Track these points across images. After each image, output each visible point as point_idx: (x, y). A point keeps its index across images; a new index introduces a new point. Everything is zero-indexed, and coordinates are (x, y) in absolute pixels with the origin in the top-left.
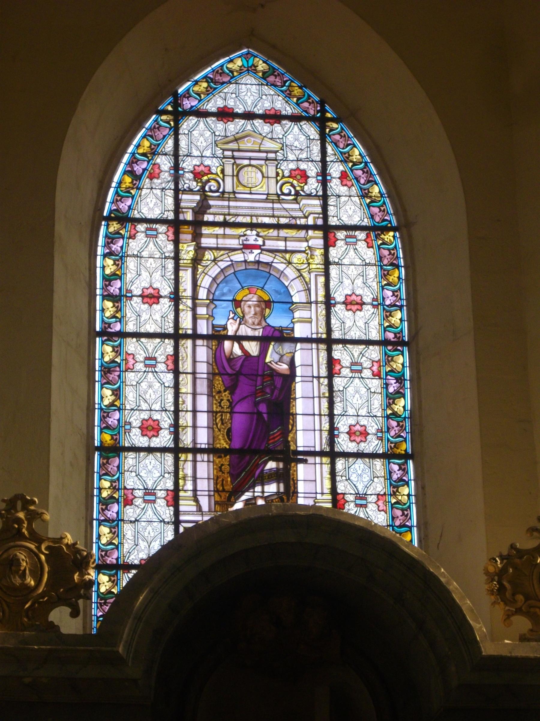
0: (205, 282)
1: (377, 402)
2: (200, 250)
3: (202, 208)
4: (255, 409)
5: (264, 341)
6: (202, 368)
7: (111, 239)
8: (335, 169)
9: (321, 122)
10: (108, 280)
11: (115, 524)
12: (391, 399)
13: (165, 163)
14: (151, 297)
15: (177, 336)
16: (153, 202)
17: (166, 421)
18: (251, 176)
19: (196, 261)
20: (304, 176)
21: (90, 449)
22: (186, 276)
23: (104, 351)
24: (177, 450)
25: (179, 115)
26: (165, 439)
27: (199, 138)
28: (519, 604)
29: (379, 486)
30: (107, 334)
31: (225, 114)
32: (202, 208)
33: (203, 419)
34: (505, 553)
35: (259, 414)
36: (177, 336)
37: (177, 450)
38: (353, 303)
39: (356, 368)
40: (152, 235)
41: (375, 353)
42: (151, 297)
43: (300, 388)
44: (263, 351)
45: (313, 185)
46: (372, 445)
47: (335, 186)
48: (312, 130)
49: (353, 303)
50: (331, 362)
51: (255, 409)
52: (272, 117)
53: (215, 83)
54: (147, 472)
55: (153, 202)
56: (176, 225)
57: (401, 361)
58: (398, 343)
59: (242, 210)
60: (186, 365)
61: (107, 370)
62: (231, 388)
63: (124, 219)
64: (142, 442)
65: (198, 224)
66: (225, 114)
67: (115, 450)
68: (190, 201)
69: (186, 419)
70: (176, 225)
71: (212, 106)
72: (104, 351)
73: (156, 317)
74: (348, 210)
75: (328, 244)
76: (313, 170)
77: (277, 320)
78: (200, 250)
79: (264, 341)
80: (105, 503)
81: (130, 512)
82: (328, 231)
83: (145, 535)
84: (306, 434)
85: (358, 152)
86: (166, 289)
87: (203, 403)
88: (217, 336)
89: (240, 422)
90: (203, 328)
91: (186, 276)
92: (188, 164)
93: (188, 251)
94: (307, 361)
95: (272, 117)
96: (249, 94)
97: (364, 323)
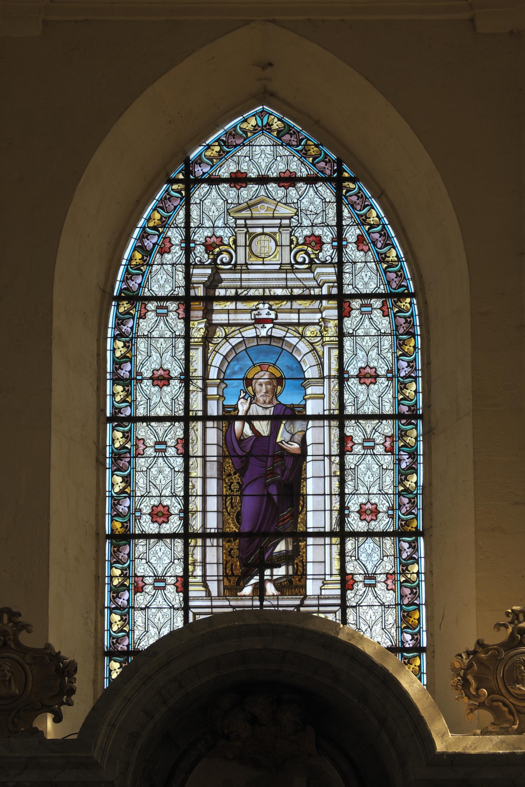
0: (217, 360)
1: (389, 478)
2: (211, 327)
3: (214, 282)
5: (275, 420)
6: (212, 451)
7: (120, 321)
8: (352, 234)
9: (337, 182)
10: (118, 363)
11: (126, 612)
12: (402, 475)
13: (176, 236)
14: (161, 379)
15: (187, 419)
16: (163, 280)
17: (176, 507)
18: (264, 246)
19: (207, 339)
20: (317, 242)
21: (100, 536)
22: (197, 355)
23: (115, 437)
24: (186, 536)
25: (190, 183)
26: (174, 524)
27: (211, 205)
28: (482, 699)
29: (388, 566)
30: (117, 419)
31: (238, 180)
32: (214, 282)
33: (212, 504)
34: (472, 649)
35: (269, 496)
36: (187, 419)
37: (186, 536)
38: (368, 376)
39: (369, 445)
40: (162, 316)
41: (387, 427)
42: (161, 379)
43: (310, 468)
44: (274, 431)
45: (328, 252)
46: (383, 523)
47: (352, 252)
48: (327, 192)
49: (368, 376)
50: (344, 439)
52: (287, 180)
53: (230, 144)
54: (158, 559)
55: (163, 280)
56: (186, 301)
57: (415, 434)
58: (412, 416)
59: (254, 281)
60: (196, 449)
61: (117, 456)
62: (242, 471)
63: (135, 298)
64: (152, 528)
65: (209, 299)
66: (238, 180)
67: (125, 537)
68: (201, 274)
69: (196, 504)
70: (186, 301)
71: (224, 173)
72: (115, 437)
73: (163, 400)
74: (365, 278)
75: (343, 313)
76: (327, 235)
77: (289, 398)
78: (211, 327)
79: (275, 420)
80: (116, 592)
81: (141, 600)
82: (342, 301)
83: (155, 621)
84: (317, 515)
85: (376, 212)
86: (176, 371)
87: (212, 486)
88: (228, 417)
89: (249, 506)
90: (213, 409)
91: (197, 355)
92: (199, 236)
93: (198, 330)
94: (318, 438)
95: (287, 180)
96: (263, 156)
97: (378, 397)
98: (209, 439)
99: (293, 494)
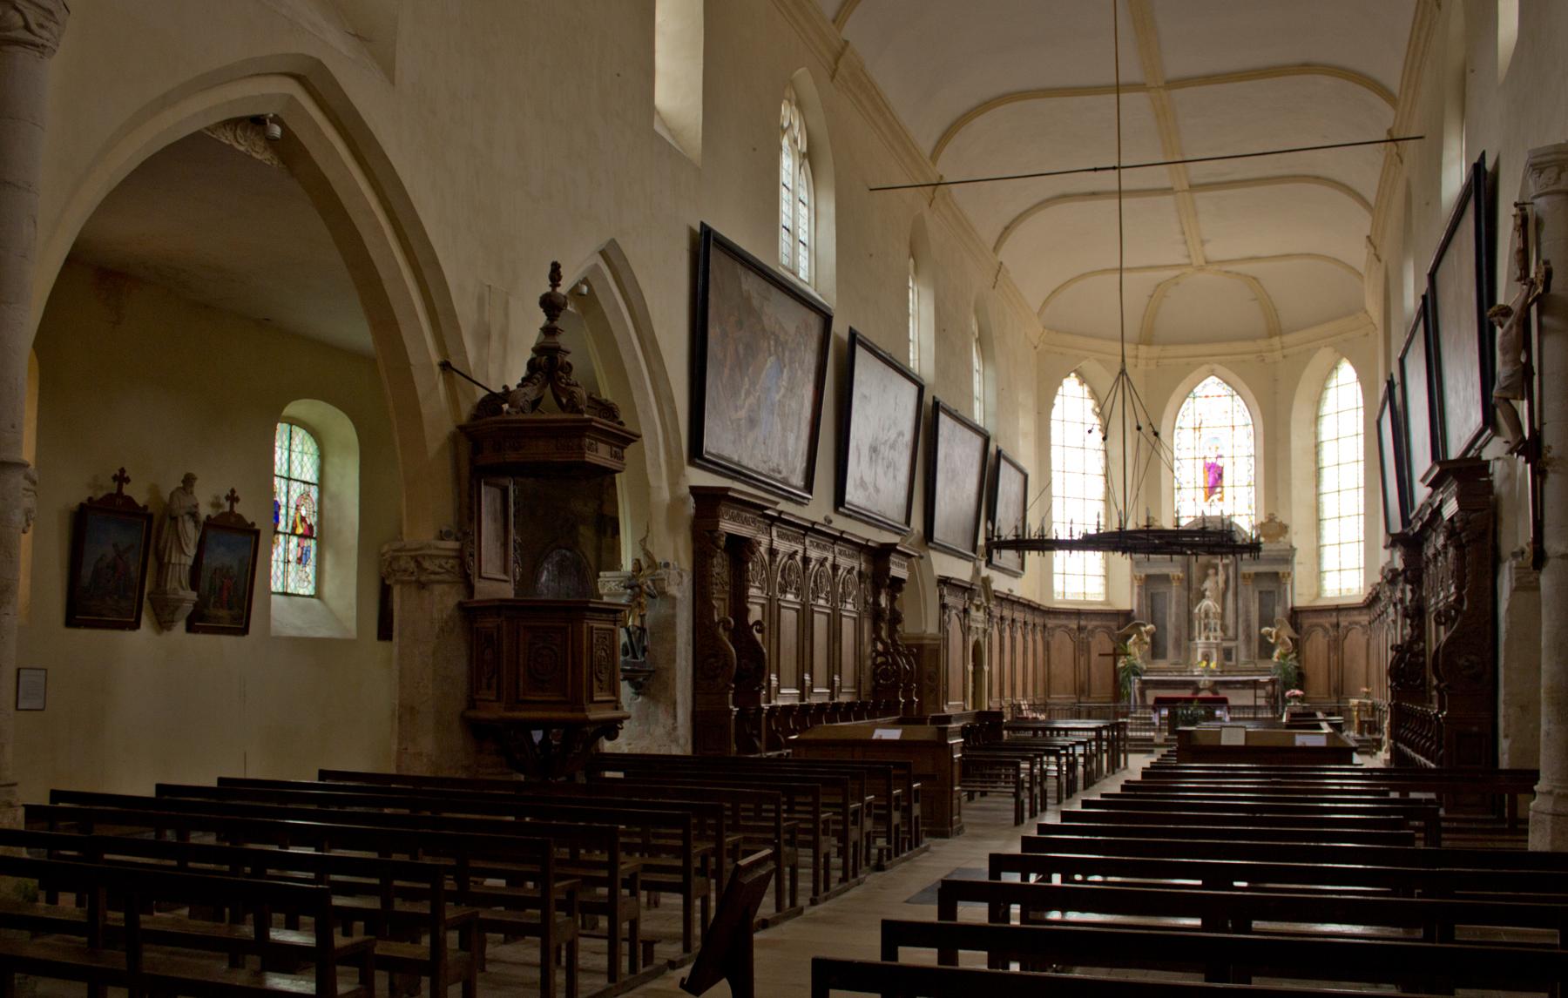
4: (1215, 478)
51: (1215, 478)
84: (1227, 479)
89: (1211, 479)
98: (1200, 464)
99: (1220, 476)
